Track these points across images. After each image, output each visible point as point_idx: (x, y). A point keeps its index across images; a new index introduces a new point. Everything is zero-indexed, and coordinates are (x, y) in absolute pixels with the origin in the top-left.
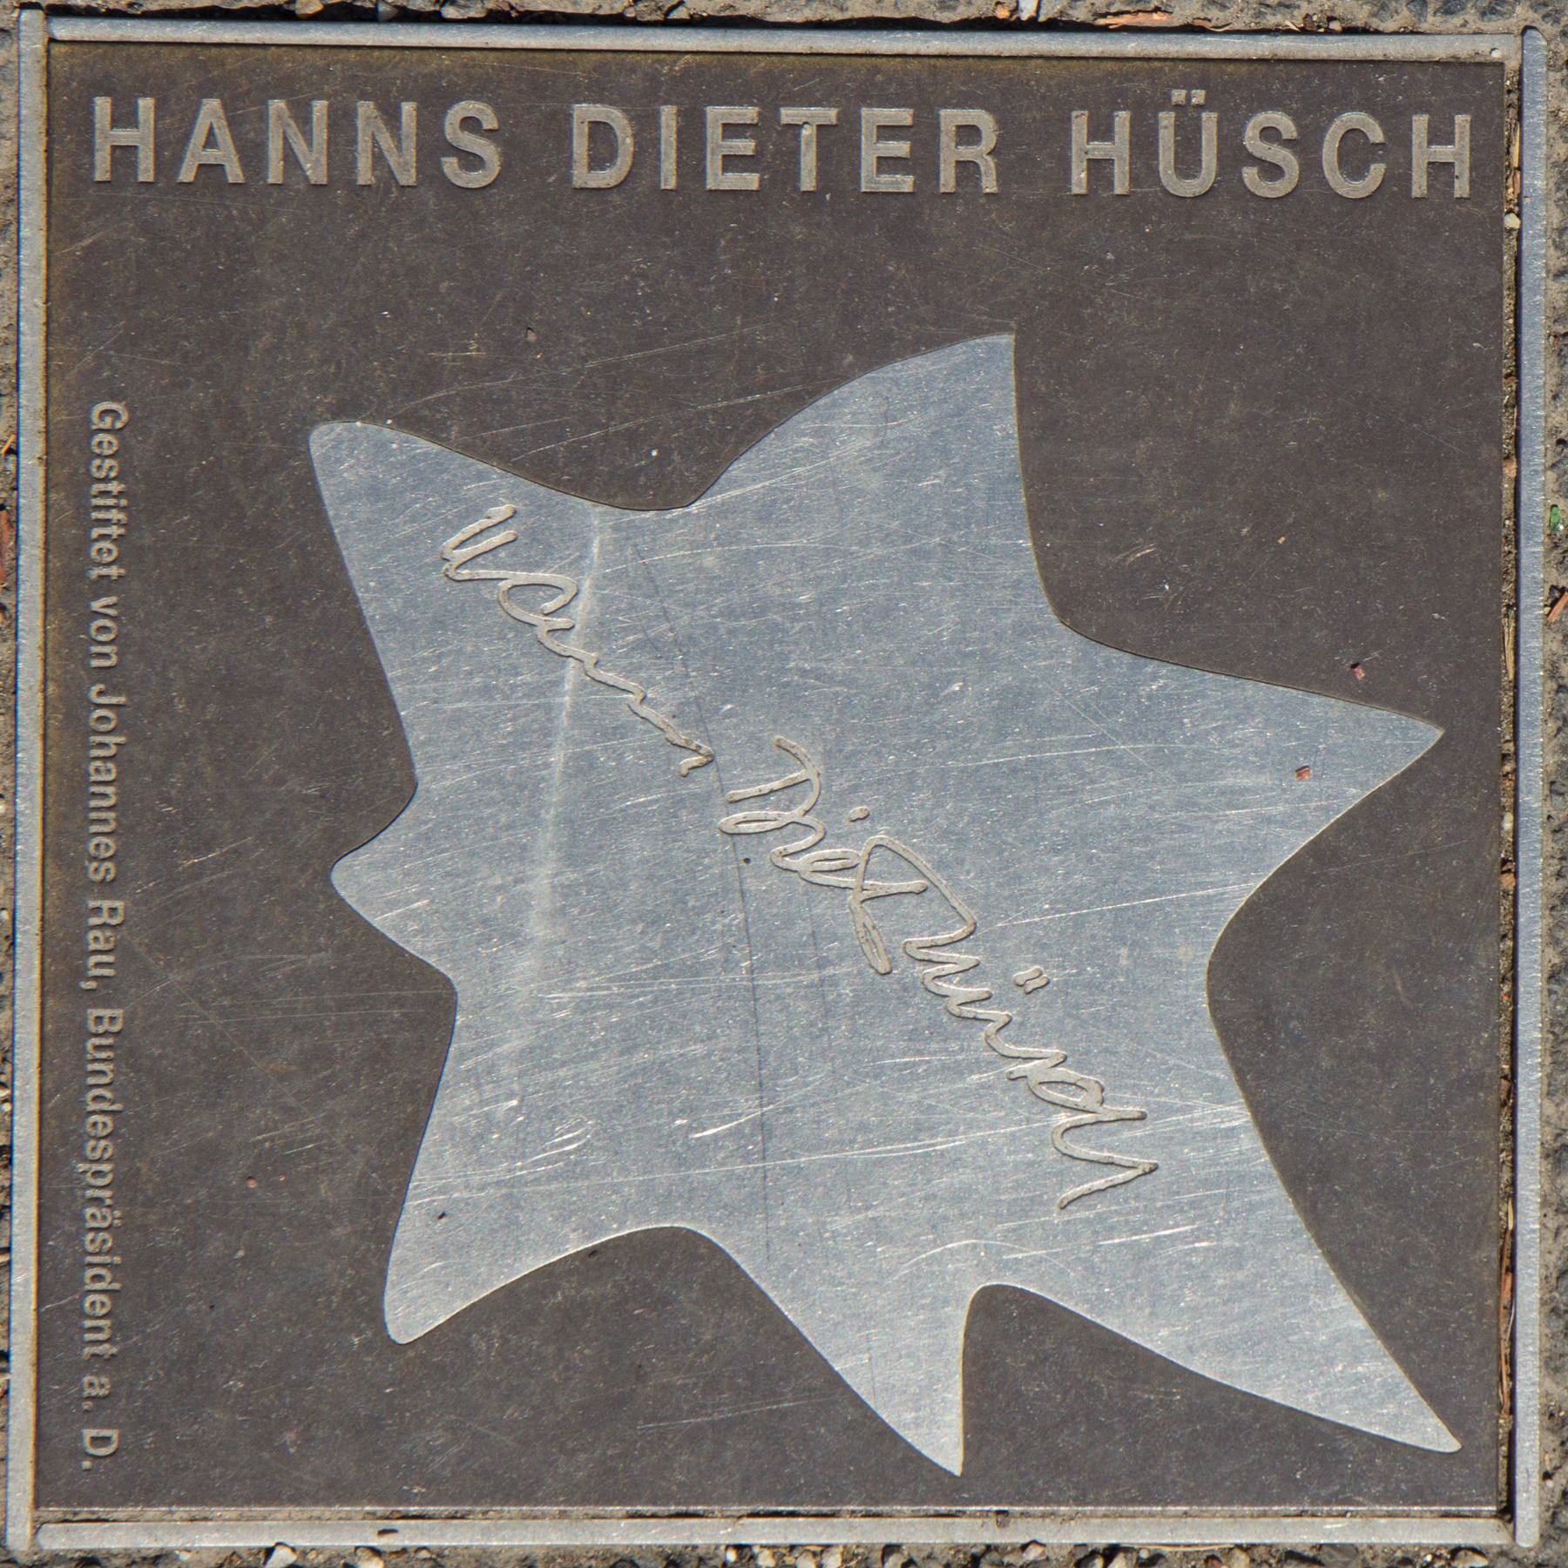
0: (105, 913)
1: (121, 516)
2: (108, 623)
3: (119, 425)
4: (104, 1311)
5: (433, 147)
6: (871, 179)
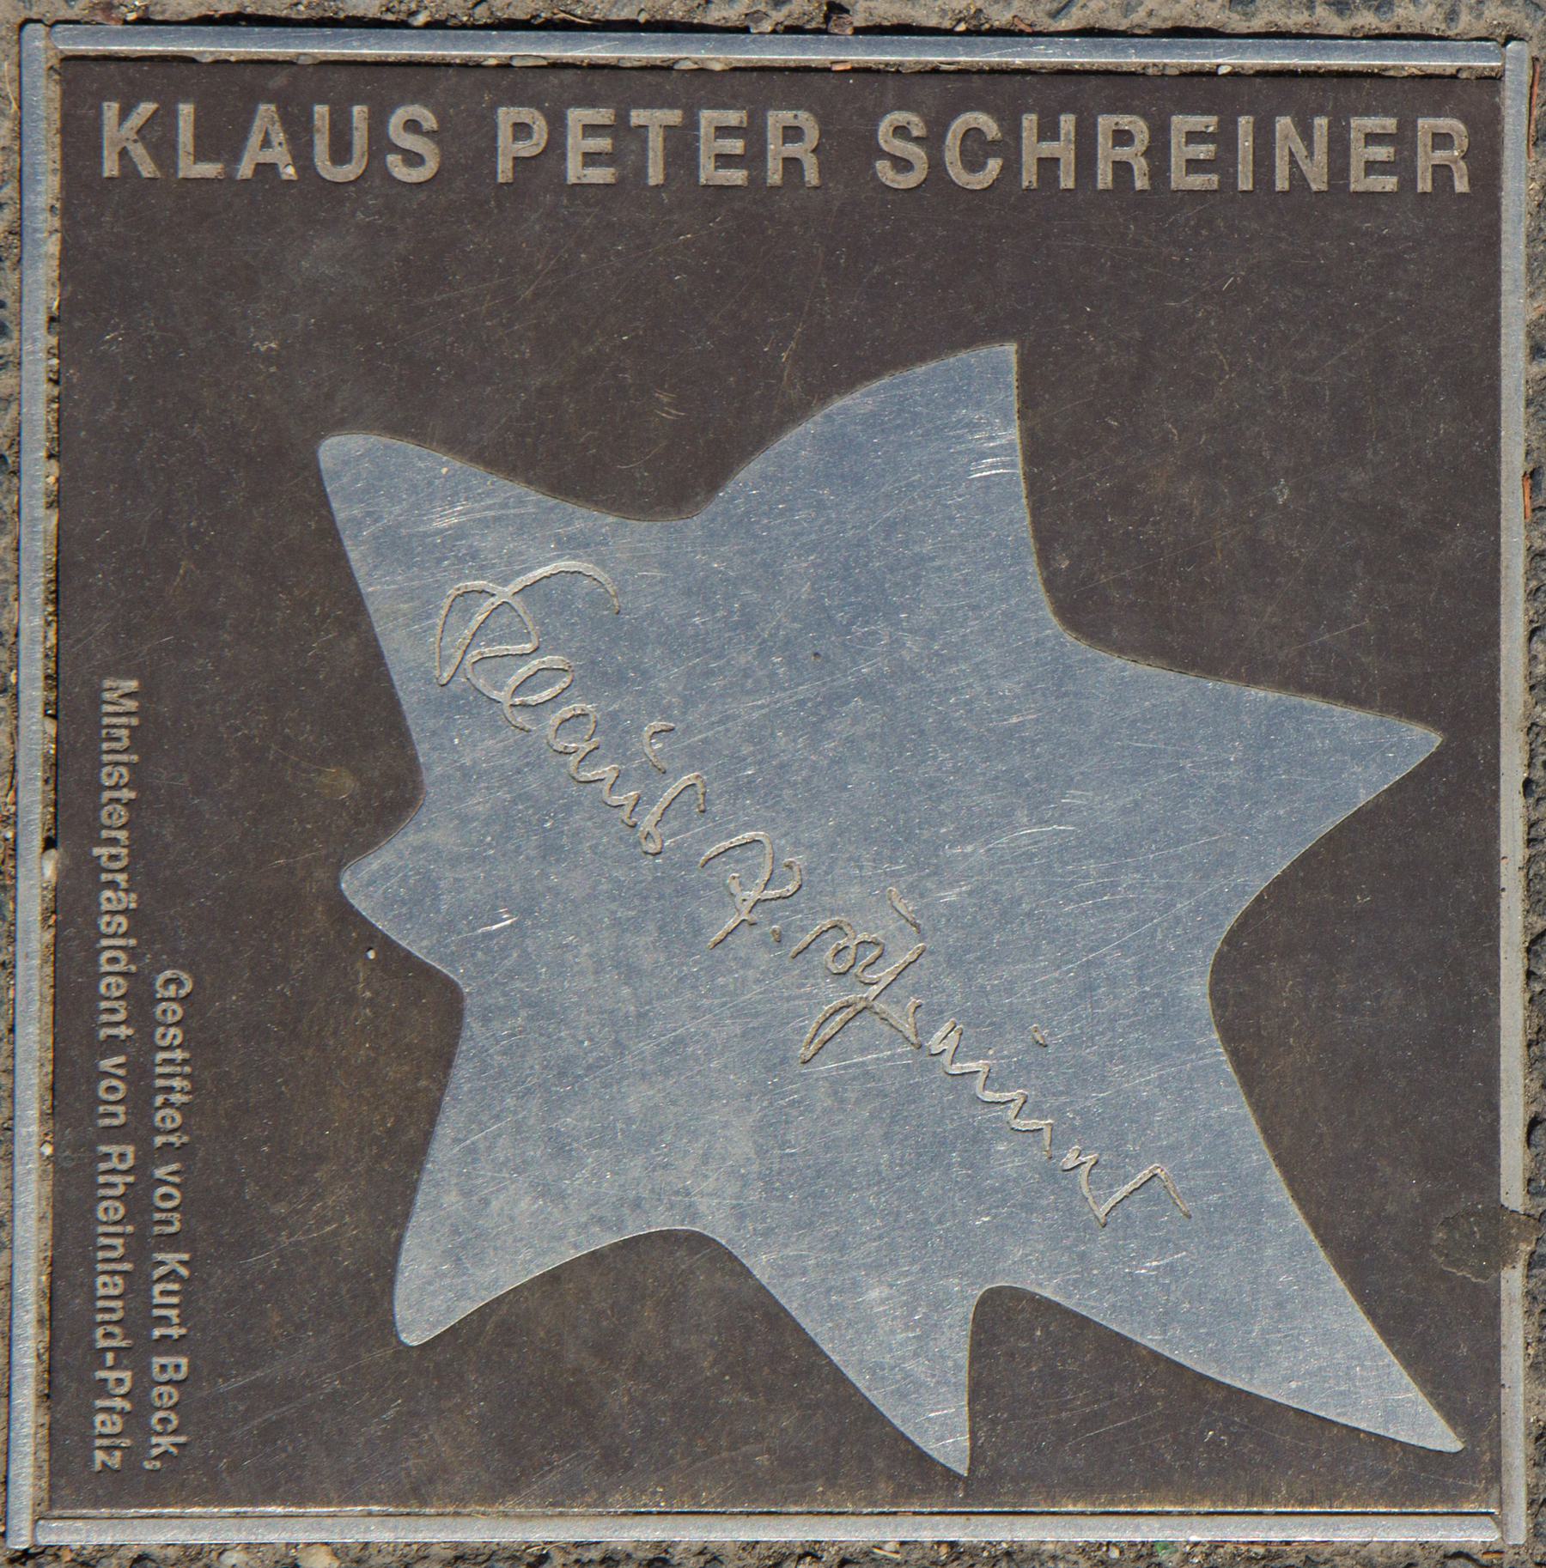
0: (115, 1159)
2: (115, 1082)
3: (183, 993)
4: (118, 994)
6: (708, 173)
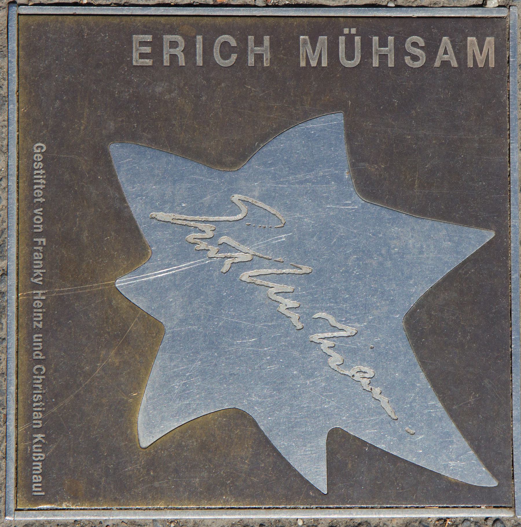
1: (45, 182)
3: (43, 151)
5: (400, 52)
